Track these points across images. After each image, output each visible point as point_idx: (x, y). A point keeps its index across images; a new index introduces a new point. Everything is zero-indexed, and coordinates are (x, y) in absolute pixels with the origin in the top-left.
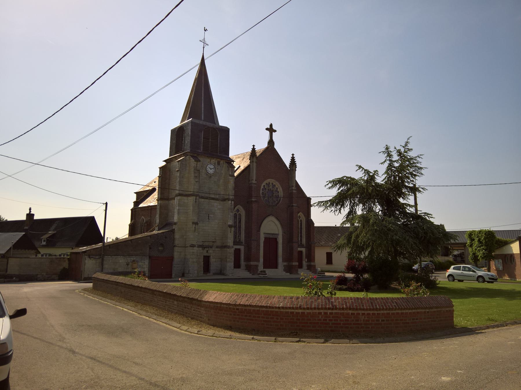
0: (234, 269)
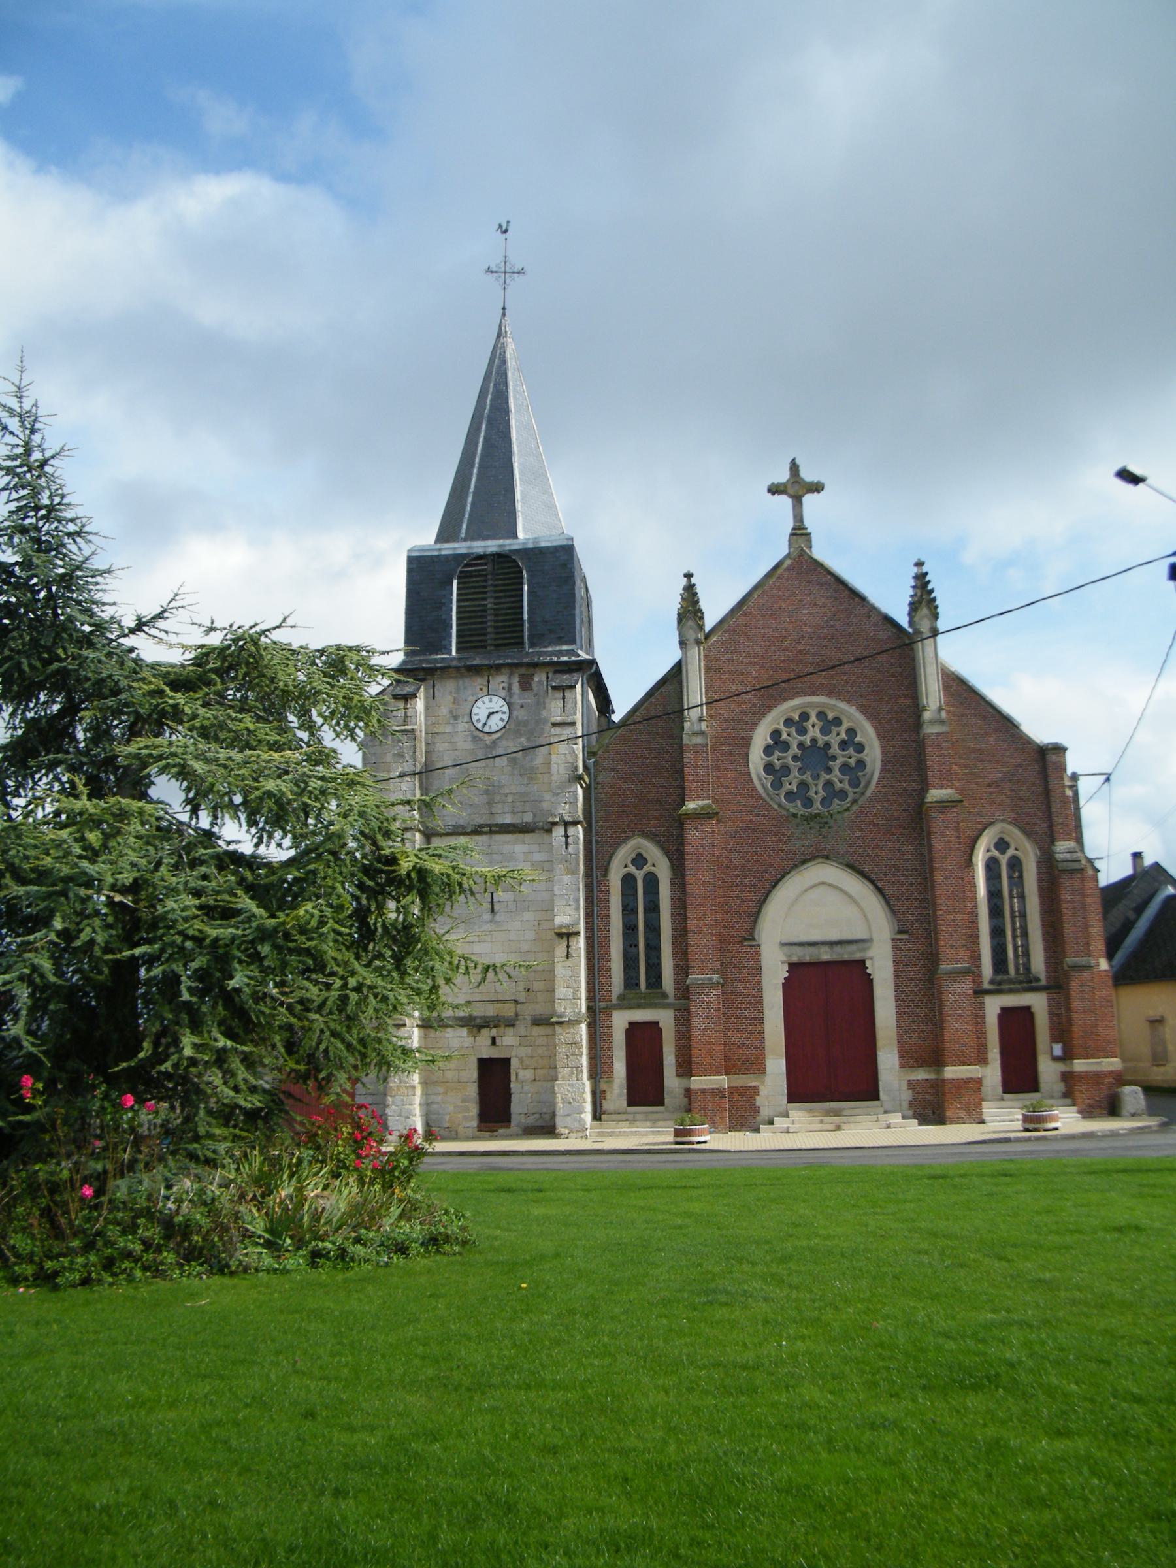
0: (1006, 1096)
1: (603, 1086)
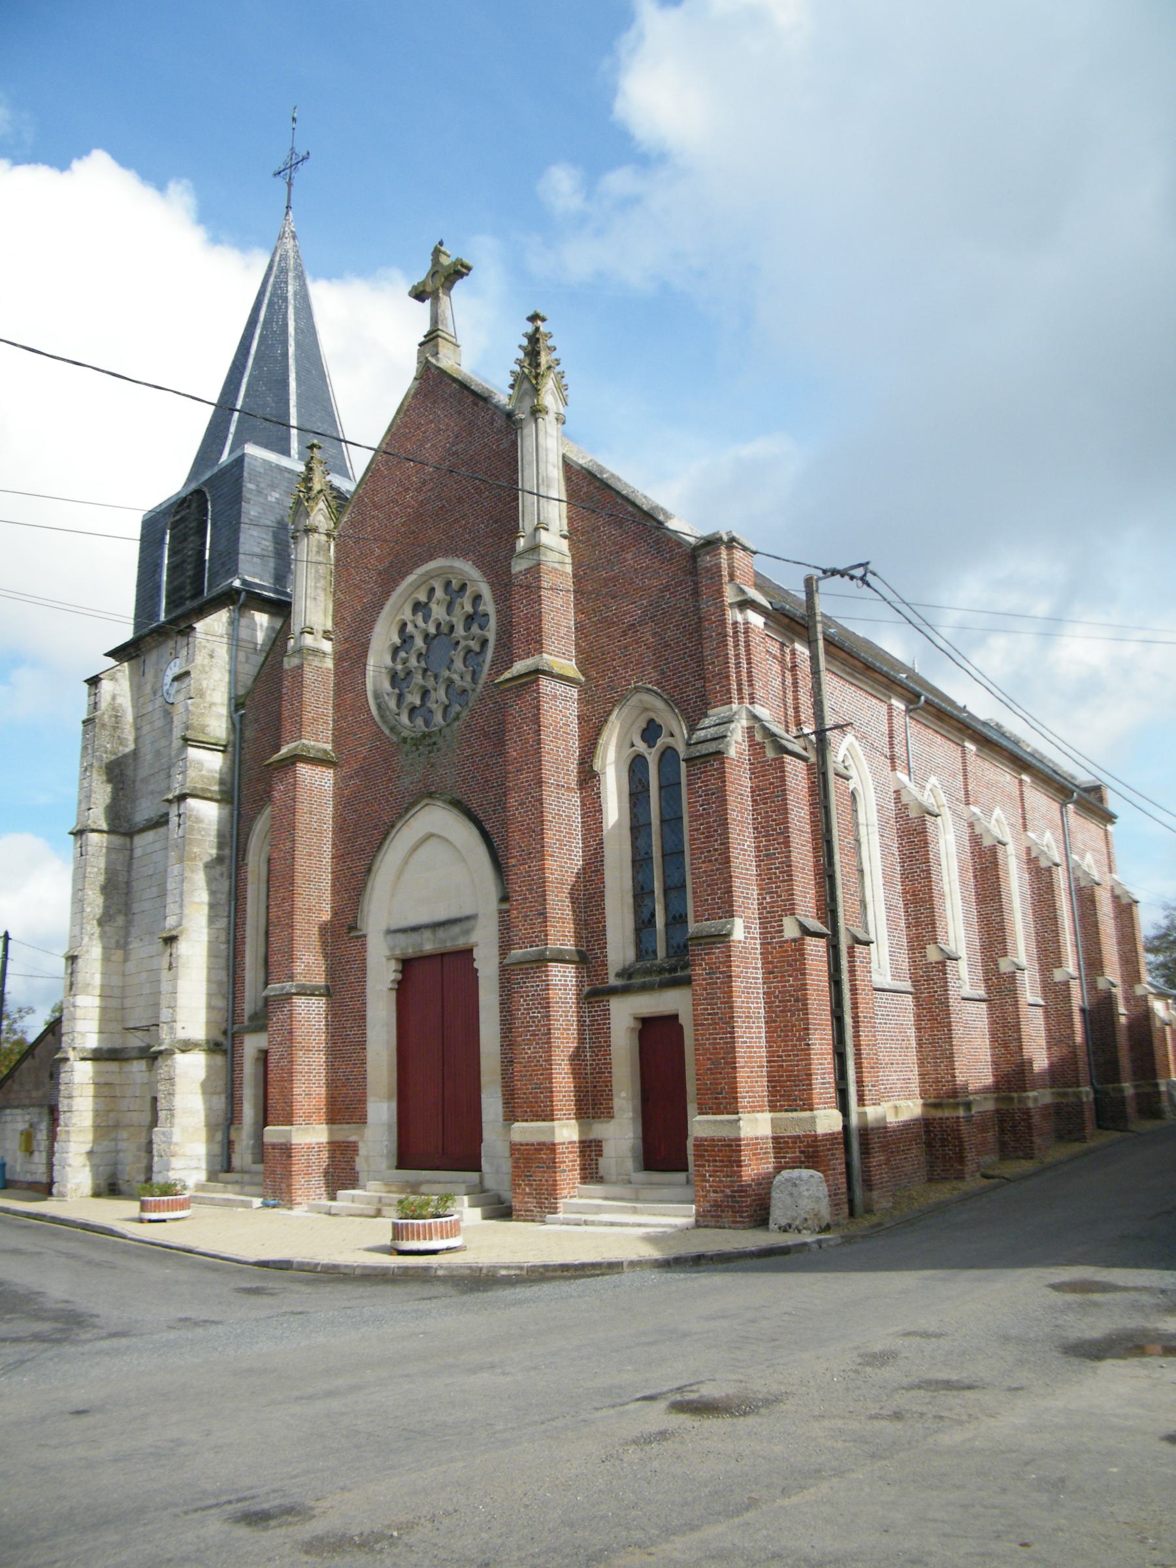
1: (233, 1136)
